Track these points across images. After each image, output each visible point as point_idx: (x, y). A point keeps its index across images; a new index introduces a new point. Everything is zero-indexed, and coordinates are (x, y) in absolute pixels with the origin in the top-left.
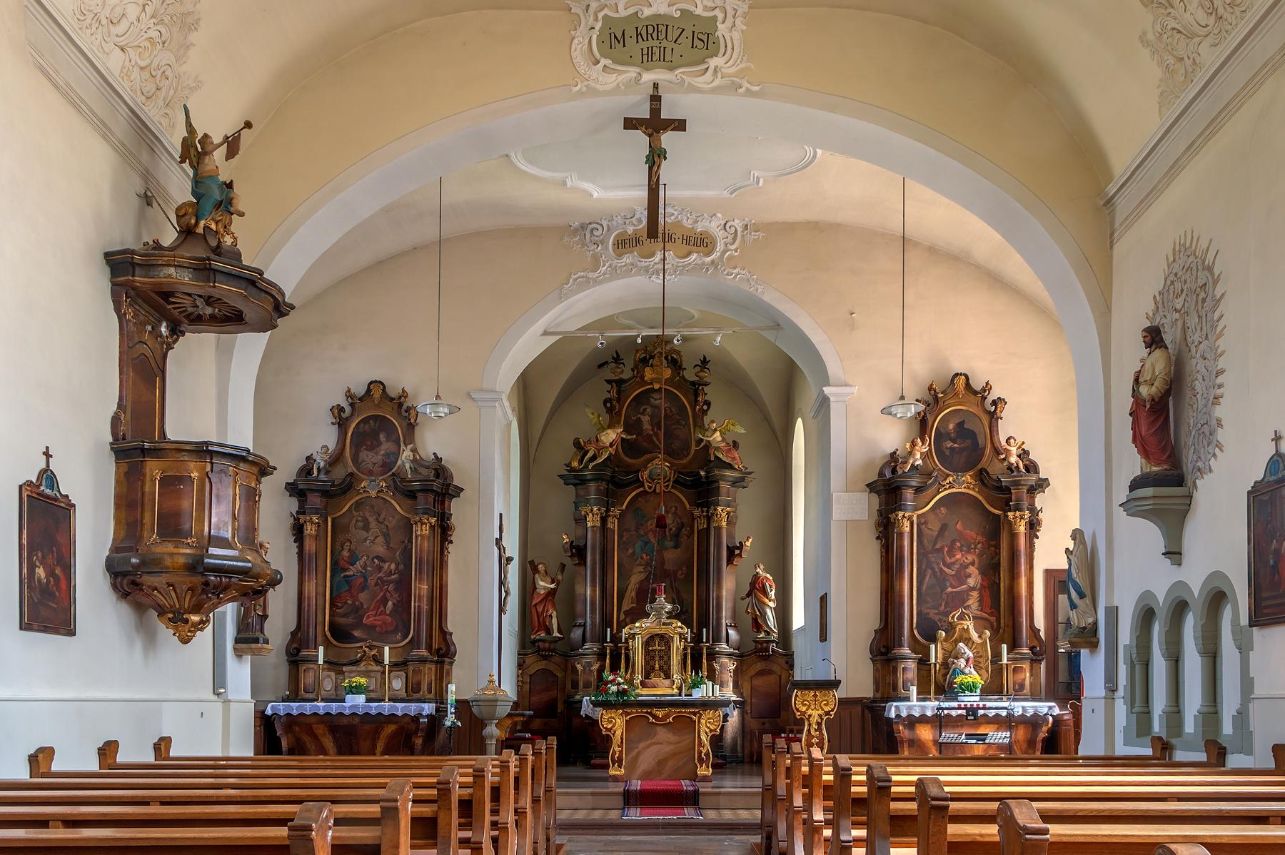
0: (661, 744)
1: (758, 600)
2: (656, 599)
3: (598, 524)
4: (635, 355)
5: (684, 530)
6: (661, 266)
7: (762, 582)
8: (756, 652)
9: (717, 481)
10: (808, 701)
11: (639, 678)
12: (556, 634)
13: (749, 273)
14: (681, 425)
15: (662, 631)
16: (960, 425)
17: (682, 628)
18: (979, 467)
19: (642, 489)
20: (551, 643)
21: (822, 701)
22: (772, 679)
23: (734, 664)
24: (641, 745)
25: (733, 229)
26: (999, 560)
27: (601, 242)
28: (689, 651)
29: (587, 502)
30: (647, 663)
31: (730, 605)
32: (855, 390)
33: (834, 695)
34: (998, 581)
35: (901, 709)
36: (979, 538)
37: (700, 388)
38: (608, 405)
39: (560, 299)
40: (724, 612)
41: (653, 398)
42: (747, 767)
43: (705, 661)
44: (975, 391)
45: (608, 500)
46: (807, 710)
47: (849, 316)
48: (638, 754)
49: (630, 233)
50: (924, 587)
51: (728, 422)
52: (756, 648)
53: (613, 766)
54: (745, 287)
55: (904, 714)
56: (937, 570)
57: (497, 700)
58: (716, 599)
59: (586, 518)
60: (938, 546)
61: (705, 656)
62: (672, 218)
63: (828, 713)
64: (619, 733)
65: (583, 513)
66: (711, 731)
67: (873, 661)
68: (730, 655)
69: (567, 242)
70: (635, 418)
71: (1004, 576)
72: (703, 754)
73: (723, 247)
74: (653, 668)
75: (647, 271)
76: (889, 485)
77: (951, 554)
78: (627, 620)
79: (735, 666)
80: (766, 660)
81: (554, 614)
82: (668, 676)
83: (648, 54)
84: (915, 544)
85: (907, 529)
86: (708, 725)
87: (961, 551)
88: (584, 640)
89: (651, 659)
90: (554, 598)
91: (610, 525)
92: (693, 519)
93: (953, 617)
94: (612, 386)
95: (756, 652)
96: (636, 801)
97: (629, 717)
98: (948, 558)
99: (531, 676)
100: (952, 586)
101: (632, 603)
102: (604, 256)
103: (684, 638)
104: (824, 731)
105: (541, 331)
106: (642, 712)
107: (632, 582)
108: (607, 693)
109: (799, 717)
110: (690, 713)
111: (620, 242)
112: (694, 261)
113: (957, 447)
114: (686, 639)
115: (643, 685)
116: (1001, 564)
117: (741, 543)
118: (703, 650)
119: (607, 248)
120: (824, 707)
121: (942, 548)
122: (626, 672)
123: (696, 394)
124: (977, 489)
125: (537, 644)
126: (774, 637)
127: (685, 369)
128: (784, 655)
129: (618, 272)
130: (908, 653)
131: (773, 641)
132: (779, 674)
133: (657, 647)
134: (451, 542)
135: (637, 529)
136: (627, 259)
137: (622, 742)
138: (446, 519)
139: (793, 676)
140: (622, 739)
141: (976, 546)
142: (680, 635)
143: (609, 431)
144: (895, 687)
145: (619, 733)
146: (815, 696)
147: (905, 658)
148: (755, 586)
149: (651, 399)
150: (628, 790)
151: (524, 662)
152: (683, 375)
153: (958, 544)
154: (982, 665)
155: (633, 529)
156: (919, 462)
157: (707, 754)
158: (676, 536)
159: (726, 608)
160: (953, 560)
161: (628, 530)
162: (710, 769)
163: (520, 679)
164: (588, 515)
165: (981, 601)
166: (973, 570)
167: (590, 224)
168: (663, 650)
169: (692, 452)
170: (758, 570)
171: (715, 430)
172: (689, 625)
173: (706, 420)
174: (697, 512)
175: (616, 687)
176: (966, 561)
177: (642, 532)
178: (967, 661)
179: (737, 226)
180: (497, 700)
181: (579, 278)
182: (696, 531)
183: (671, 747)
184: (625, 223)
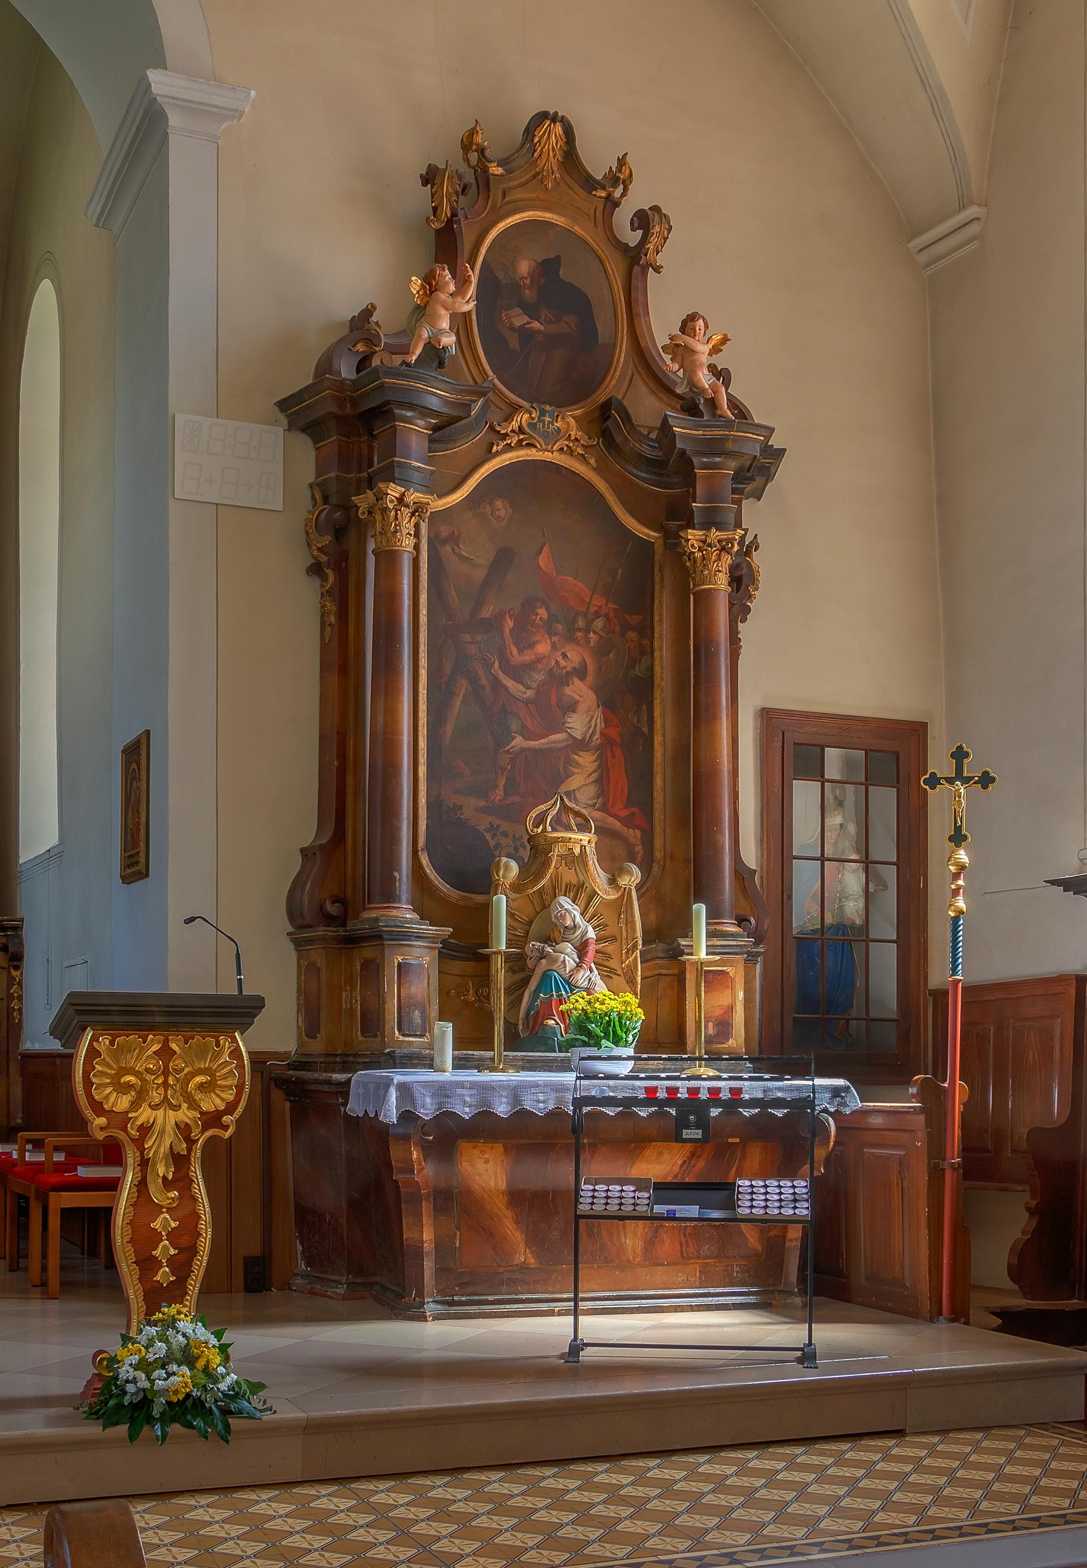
10: (137, 1074)
16: (548, 268)
18: (601, 397)
26: (651, 668)
33: (236, 1053)
34: (645, 730)
35: (417, 1095)
36: (598, 601)
44: (589, 176)
46: (135, 1105)
50: (449, 729)
55: (427, 1109)
56: (484, 682)
60: (486, 613)
63: (212, 1120)
71: (663, 715)
76: (354, 402)
77: (524, 639)
84: (423, 598)
85: (408, 543)
87: (550, 632)
93: (540, 820)
98: (515, 651)
100: (528, 735)
104: (200, 1188)
109: (100, 1136)
113: (539, 332)
116: (657, 681)
120: (198, 1096)
121: (499, 618)
124: (592, 461)
130: (411, 921)
139: (20, 984)
141: (589, 623)
144: (372, 1023)
147: (403, 936)
153: (543, 613)
154: (613, 964)
156: (449, 340)
160: (528, 657)
163: (15, 1004)
165: (603, 781)
166: (580, 691)
176: (563, 663)
178: (582, 949)
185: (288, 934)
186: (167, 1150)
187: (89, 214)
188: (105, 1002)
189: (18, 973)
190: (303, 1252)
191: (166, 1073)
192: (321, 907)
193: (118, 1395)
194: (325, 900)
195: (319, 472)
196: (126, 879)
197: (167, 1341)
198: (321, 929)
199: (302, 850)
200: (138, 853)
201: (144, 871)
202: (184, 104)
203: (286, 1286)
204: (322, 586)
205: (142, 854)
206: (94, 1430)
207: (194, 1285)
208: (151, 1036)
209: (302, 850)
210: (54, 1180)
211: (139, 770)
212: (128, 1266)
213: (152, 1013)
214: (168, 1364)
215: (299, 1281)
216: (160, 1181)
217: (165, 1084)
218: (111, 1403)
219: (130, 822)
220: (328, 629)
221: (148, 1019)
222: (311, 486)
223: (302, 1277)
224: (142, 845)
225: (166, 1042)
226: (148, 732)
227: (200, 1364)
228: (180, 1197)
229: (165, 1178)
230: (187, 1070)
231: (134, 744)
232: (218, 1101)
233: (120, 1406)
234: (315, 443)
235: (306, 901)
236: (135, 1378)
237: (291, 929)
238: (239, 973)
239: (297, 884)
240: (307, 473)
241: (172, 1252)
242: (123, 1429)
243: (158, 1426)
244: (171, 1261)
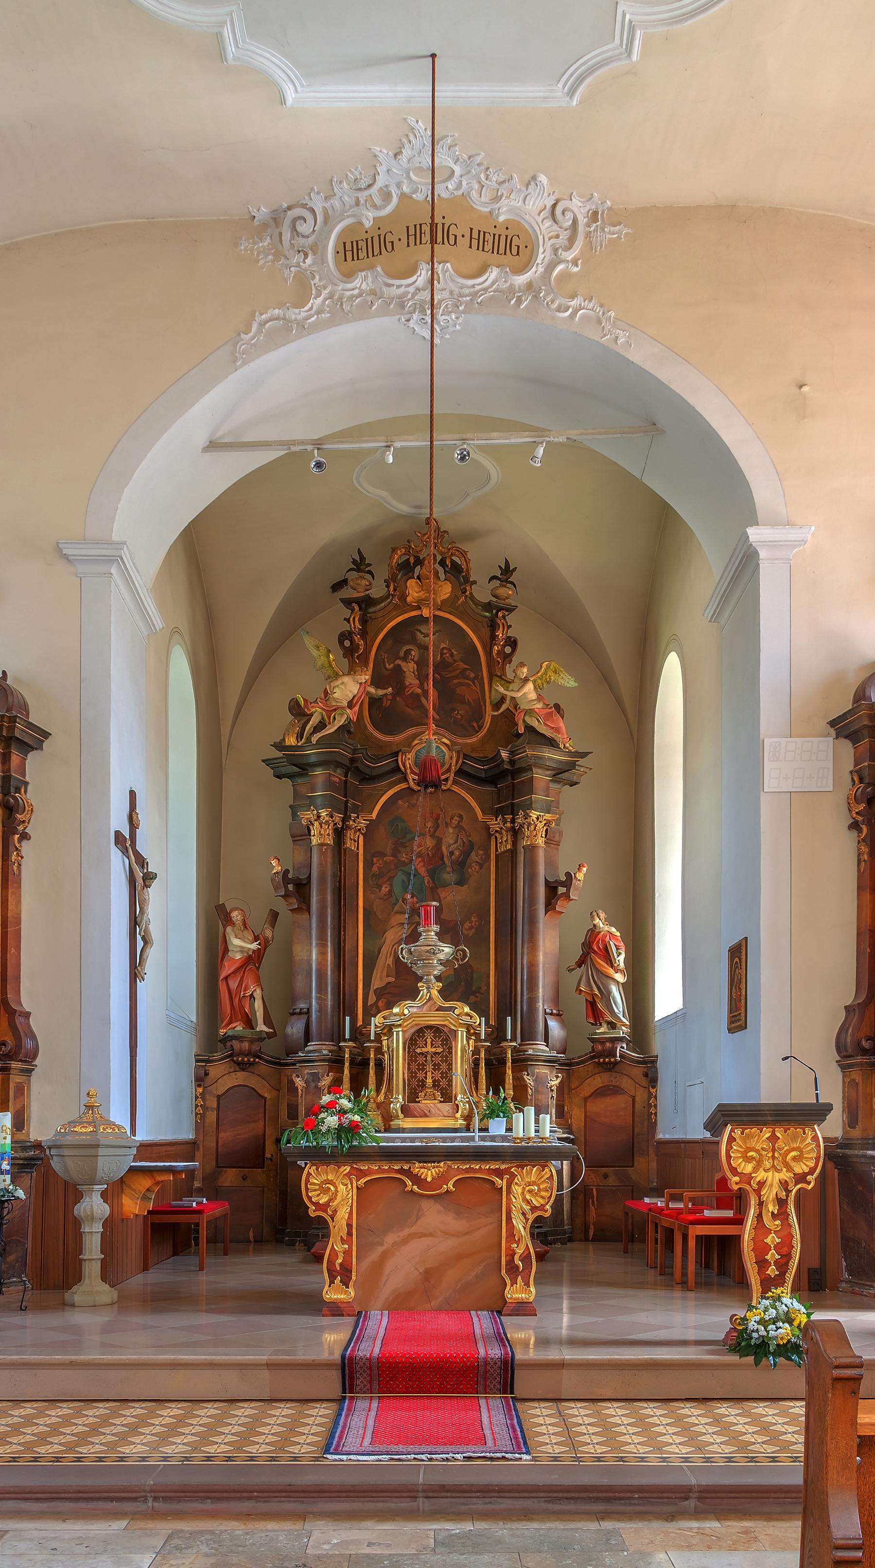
0: (431, 1235)
1: (596, 968)
2: (420, 935)
3: (330, 841)
4: (392, 558)
5: (473, 854)
6: (426, 295)
7: (603, 941)
8: (592, 1058)
9: (529, 769)
10: (757, 1151)
11: (398, 1100)
12: (261, 1027)
13: (601, 306)
14: (468, 678)
15: (435, 1019)
17: (471, 1017)
19: (403, 786)
20: (252, 1041)
21: (789, 1151)
22: (620, 1102)
23: (557, 1077)
24: (390, 1239)
25: (570, 215)
27: (311, 249)
28: (483, 1055)
29: (312, 801)
30: (412, 1075)
31: (550, 979)
32: (808, 533)
33: (815, 1138)
37: (500, 614)
38: (347, 643)
39: (234, 363)
40: (541, 990)
41: (420, 632)
42: (577, 1245)
43: (509, 1072)
45: (347, 802)
46: (755, 1169)
47: (798, 390)
48: (385, 1256)
49: (368, 224)
51: (548, 667)
52: (593, 1051)
53: (332, 1282)
54: (593, 334)
57: (97, 1146)
58: (529, 968)
59: (309, 830)
61: (509, 1064)
62: (451, 185)
63: (801, 1178)
64: (343, 1214)
65: (304, 822)
66: (534, 1209)
67: (843, 1067)
68: (551, 1061)
69: (245, 249)
70: (392, 666)
72: (516, 1257)
73: (549, 256)
74: (423, 1085)
75: (402, 305)
78: (380, 1004)
79: (559, 1080)
80: (610, 1070)
81: (258, 994)
82: (447, 1097)
83: (415, 235)
86: (528, 1197)
88: (307, 1038)
89: (419, 1070)
90: (258, 968)
91: (349, 844)
92: (490, 835)
94: (353, 610)
95: (592, 1058)
96: (370, 1382)
97: (363, 1181)
99: (219, 1097)
101: (387, 976)
102: (317, 277)
103: (475, 1034)
104: (794, 1219)
105: (202, 440)
106: (391, 1170)
107: (388, 941)
108: (316, 1133)
109: (736, 1187)
110: (491, 1171)
111: (349, 247)
112: (493, 283)
114: (477, 1035)
115: (406, 1111)
117: (568, 875)
118: (506, 1053)
119: (323, 260)
120: (793, 1164)
122: (378, 1091)
123: (493, 626)
125: (229, 1044)
126: (623, 1031)
127: (475, 582)
128: (638, 1062)
129: (347, 307)
131: (621, 1039)
132: (632, 1093)
133: (429, 1049)
134: (25, 836)
135: (395, 853)
136: (362, 282)
137: (350, 1234)
138: (12, 790)
139: (656, 1097)
140: (349, 1226)
142: (468, 1027)
143: (346, 679)
145: (343, 1214)
146: (773, 1138)
148: (590, 947)
149: (418, 634)
150: (351, 1358)
151: (206, 1074)
152: (471, 594)
155: (388, 851)
157: (526, 1258)
158: (461, 865)
159: (544, 983)
161: (382, 855)
162: (532, 1289)
163: (652, 1110)
164: (313, 825)
167: (289, 208)
168: (438, 1053)
169: (488, 720)
170: (597, 921)
171: (526, 680)
172: (482, 1011)
173: (509, 669)
174: (495, 824)
175: (336, 1118)
177: (404, 858)
179: (576, 210)
180: (97, 1146)
181: (270, 320)
182: (493, 856)
183: (451, 1242)
184: (357, 203)
185: (837, 1062)
186: (775, 1196)
187: (706, 615)
188: (739, 1109)
189: (655, 1090)
190: (847, 1266)
191: (774, 1150)
192: (859, 1043)
193: (747, 1339)
194: (861, 1040)
195: (857, 762)
196: (731, 1030)
197: (776, 1309)
198: (859, 1058)
199: (846, 1007)
200: (740, 1014)
201: (744, 1025)
202: (769, 543)
203: (835, 1288)
204: (859, 836)
205: (743, 1015)
206: (735, 1358)
207: (790, 1277)
208: (765, 1129)
209: (846, 1007)
210: (691, 1217)
211: (740, 962)
212: (751, 1265)
213: (766, 1115)
214: (777, 1322)
215: (844, 1285)
216: (770, 1214)
217: (773, 1157)
218: (743, 1344)
219: (734, 995)
220: (863, 864)
221: (763, 1118)
222: (851, 772)
223: (846, 1282)
224: (743, 1009)
225: (773, 1132)
226: (746, 938)
227: (796, 1323)
228: (782, 1225)
229: (772, 1212)
230: (786, 1148)
231: (737, 946)
232: (804, 1167)
233: (749, 1345)
234: (854, 744)
235: (849, 1040)
236: (757, 1329)
237: (839, 1059)
238: (817, 1090)
239: (843, 1029)
240: (849, 765)
241: (777, 1257)
242: (751, 1359)
243: (771, 1358)
244: (776, 1262)
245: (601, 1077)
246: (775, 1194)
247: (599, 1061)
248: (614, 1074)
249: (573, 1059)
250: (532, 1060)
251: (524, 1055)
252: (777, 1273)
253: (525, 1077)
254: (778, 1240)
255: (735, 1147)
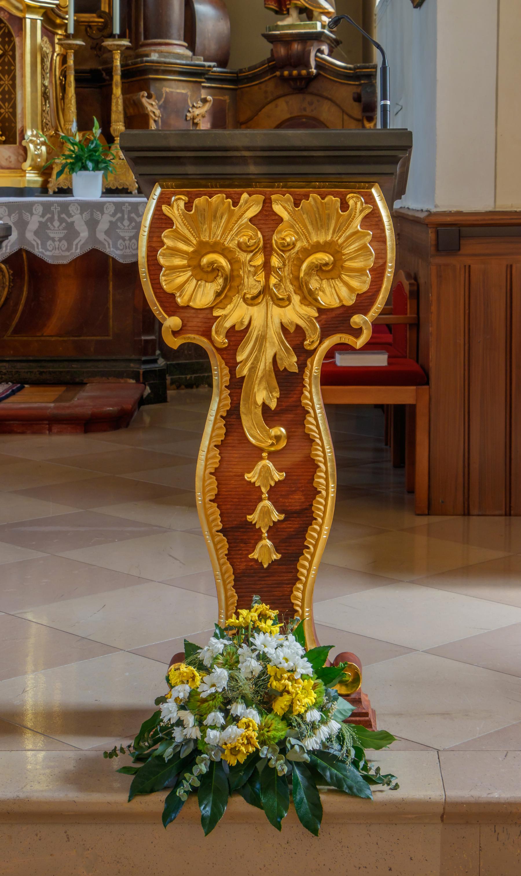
8: (273, 69)
10: (224, 252)
21: (307, 252)
23: (205, 101)
43: (117, 91)
61: (117, 78)
95: (273, 69)
118: (111, 60)
128: (348, 77)
131: (318, 37)
208: (245, 196)
212: (213, 537)
216: (259, 411)
217: (267, 266)
225: (267, 203)
228: (289, 437)
241: (276, 516)
245: (287, 103)
246: (270, 359)
247: (282, 76)
248: (309, 98)
249: (241, 71)
250: (157, 72)
251: (142, 62)
252: (276, 556)
253: (145, 101)
254: (278, 476)
255: (168, 242)
